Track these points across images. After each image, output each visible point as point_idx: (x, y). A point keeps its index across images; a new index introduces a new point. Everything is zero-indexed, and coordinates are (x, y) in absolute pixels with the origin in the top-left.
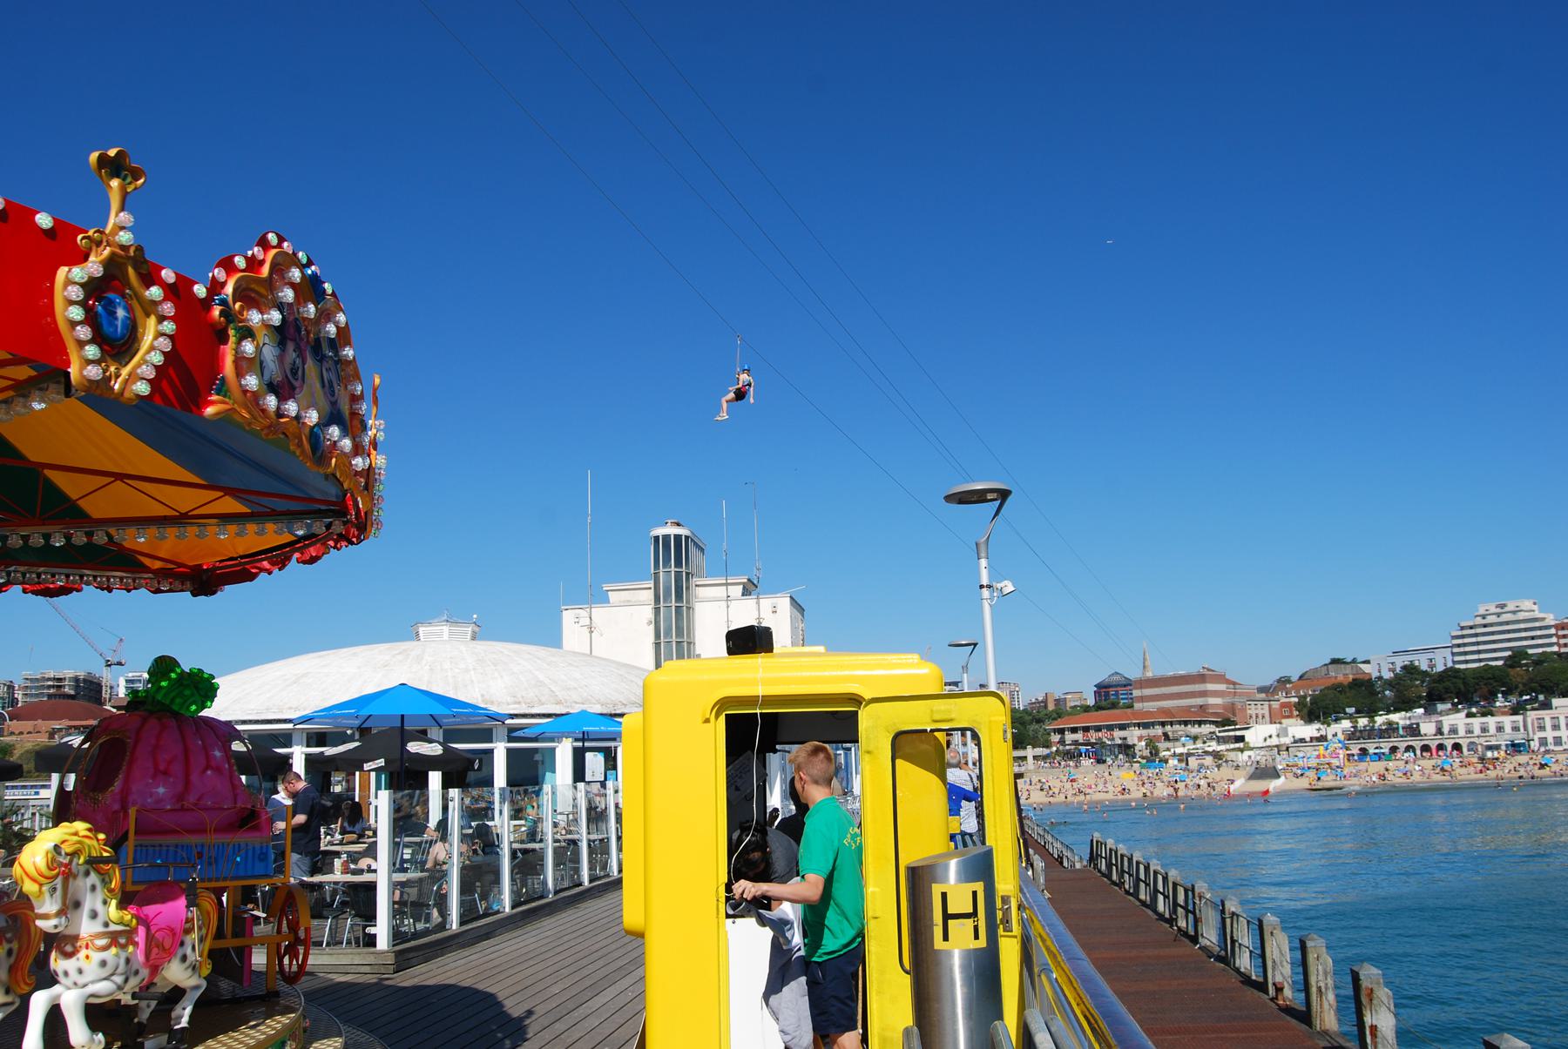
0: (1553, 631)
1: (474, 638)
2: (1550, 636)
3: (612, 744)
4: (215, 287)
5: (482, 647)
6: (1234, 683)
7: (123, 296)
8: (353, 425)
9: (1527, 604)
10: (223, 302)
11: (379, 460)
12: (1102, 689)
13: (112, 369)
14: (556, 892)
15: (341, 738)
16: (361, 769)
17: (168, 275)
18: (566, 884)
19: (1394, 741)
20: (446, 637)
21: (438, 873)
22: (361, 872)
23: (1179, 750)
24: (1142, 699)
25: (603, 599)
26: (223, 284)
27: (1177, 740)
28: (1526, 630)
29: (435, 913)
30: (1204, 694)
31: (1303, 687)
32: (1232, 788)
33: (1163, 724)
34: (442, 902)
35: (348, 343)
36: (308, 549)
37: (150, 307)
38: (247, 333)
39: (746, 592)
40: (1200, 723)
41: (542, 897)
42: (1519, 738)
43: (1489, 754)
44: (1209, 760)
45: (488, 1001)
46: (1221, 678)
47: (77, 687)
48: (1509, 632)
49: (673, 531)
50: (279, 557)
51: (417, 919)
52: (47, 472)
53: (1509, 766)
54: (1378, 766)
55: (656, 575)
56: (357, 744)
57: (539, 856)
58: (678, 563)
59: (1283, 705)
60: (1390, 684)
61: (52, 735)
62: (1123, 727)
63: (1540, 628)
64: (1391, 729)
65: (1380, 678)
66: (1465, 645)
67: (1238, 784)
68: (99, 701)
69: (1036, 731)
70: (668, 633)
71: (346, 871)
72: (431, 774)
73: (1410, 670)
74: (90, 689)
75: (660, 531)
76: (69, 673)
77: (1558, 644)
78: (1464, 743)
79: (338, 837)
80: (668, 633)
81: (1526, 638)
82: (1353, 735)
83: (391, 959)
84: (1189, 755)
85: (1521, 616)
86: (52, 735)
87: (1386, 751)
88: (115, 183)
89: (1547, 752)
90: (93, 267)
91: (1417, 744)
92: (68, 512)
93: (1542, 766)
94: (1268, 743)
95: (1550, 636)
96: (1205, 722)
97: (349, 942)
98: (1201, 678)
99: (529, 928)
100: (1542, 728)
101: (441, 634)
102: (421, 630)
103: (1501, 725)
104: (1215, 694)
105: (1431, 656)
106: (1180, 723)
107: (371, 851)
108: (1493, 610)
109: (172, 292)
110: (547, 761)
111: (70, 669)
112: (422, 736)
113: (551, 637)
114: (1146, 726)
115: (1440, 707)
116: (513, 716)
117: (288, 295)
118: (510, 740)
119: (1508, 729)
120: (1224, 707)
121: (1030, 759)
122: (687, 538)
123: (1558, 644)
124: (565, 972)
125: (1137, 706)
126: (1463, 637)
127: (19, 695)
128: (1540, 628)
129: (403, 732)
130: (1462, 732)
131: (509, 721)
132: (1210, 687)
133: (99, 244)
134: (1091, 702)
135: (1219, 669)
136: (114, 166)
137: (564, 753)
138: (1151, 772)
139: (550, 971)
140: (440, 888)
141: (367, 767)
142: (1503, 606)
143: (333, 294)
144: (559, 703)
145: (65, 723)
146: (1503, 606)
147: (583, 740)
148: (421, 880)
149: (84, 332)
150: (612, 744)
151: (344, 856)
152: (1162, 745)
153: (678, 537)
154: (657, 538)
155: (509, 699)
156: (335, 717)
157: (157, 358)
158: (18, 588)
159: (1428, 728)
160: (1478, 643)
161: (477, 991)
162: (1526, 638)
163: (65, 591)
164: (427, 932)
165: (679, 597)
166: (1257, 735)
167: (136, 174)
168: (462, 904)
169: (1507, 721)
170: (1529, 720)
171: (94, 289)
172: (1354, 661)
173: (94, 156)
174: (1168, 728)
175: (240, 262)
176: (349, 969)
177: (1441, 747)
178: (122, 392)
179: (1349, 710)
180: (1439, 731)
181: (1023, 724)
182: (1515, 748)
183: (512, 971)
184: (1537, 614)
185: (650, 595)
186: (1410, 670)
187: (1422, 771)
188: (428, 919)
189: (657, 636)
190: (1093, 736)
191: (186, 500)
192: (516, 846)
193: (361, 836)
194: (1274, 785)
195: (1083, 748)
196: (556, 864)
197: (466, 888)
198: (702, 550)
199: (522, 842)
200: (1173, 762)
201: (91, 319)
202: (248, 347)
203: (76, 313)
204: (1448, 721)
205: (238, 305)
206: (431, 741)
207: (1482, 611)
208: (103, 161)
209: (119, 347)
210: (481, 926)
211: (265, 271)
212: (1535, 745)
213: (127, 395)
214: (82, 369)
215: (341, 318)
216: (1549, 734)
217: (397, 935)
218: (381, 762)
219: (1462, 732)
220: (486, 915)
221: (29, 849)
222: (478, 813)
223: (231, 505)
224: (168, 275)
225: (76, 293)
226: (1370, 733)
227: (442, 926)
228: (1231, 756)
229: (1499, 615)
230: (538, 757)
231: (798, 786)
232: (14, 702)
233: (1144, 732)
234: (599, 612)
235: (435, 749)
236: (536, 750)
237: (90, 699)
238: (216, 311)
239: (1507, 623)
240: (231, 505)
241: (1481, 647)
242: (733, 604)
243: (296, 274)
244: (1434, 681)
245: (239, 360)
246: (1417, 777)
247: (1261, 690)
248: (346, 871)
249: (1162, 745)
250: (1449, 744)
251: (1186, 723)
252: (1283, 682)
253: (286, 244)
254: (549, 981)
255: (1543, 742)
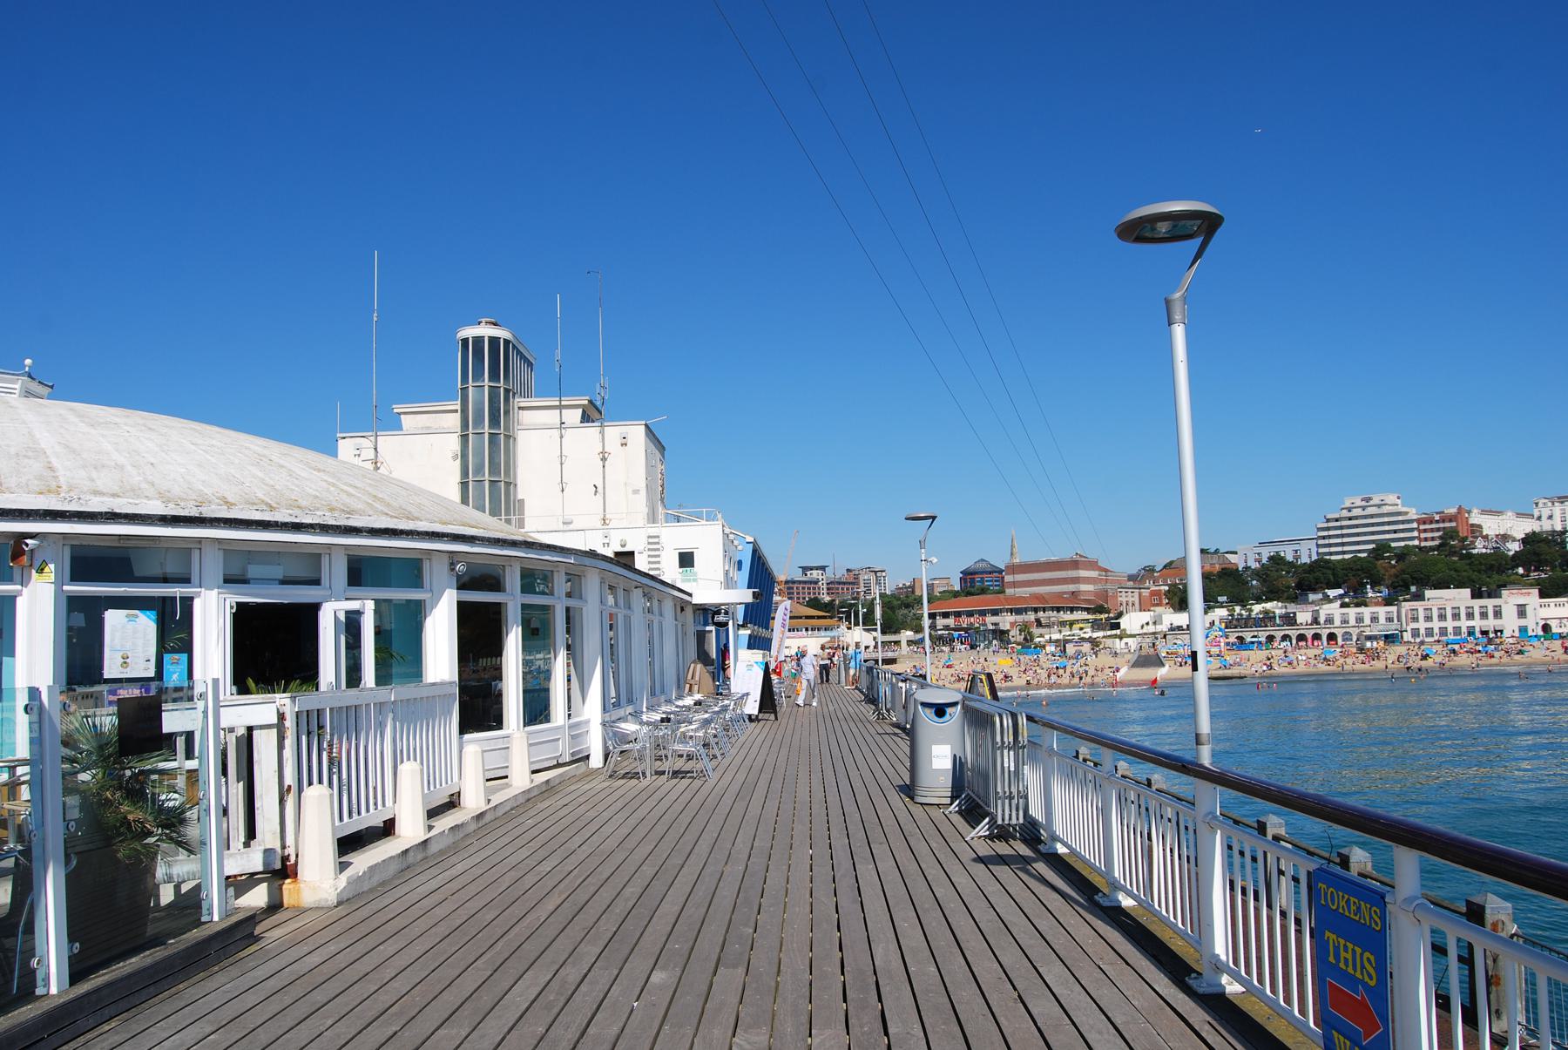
0: (1415, 525)
2: (1412, 530)
3: (177, 591)
6: (1106, 571)
9: (1391, 498)
12: (968, 576)
19: (1270, 630)
23: (1056, 636)
24: (1014, 584)
25: (394, 425)
27: (1048, 626)
28: (1389, 523)
30: (1076, 580)
31: (1169, 576)
32: (1119, 675)
33: (1036, 610)
39: (586, 418)
40: (1072, 610)
42: (1392, 629)
43: (1368, 644)
44: (1086, 647)
46: (1093, 565)
48: (1373, 525)
49: (486, 331)
53: (1391, 658)
54: (1262, 654)
55: (464, 390)
58: (494, 375)
59: (1153, 593)
60: (1257, 574)
62: (995, 613)
63: (1403, 522)
64: (1268, 618)
65: (1247, 568)
66: (1330, 537)
67: (1123, 671)
69: (905, 616)
70: (479, 469)
73: (1276, 560)
75: (470, 332)
77: (1418, 538)
78: (1339, 633)
80: (479, 469)
81: (1388, 532)
82: (1231, 623)
84: (1066, 641)
85: (1386, 509)
87: (1263, 639)
89: (1422, 643)
91: (1294, 633)
93: (1425, 657)
94: (1146, 630)
95: (1412, 530)
96: (1077, 609)
98: (1074, 564)
100: (1415, 619)
103: (1376, 615)
104: (1087, 580)
105: (1296, 547)
106: (1052, 609)
108: (1359, 503)
114: (1018, 611)
115: (1312, 597)
119: (1382, 620)
120: (1096, 594)
121: (904, 644)
122: (507, 342)
123: (1418, 538)
125: (1009, 591)
126: (1328, 529)
128: (1403, 522)
130: (1337, 622)
132: (1083, 573)
134: (957, 587)
135: (1092, 556)
138: (1025, 659)
142: (1368, 500)
146: (1368, 500)
150: (177, 591)
152: (1036, 631)
153: (494, 341)
154: (465, 341)
159: (1303, 617)
160: (1343, 536)
162: (1388, 532)
165: (494, 421)
166: (1133, 621)
169: (1382, 611)
170: (1403, 611)
172: (1217, 551)
174: (1041, 614)
177: (1317, 637)
179: (1220, 599)
180: (1316, 621)
181: (892, 608)
182: (1390, 639)
184: (1401, 509)
185: (454, 420)
186: (1276, 560)
187: (1305, 660)
189: (465, 473)
190: (965, 621)
194: (1161, 673)
195: (956, 634)
198: (530, 364)
200: (1050, 648)
204: (1325, 610)
207: (1348, 505)
212: (1407, 636)
216: (1422, 625)
219: (1337, 622)
226: (1247, 622)
228: (1109, 642)
229: (1364, 508)
231: (658, 455)
233: (1020, 618)
234: (387, 442)
239: (1372, 516)
241: (1346, 540)
242: (568, 434)
244: (1305, 572)
246: (1301, 668)
247: (1131, 578)
249: (1036, 631)
250: (1324, 633)
251: (1058, 609)
252: (1150, 570)
255: (1416, 633)
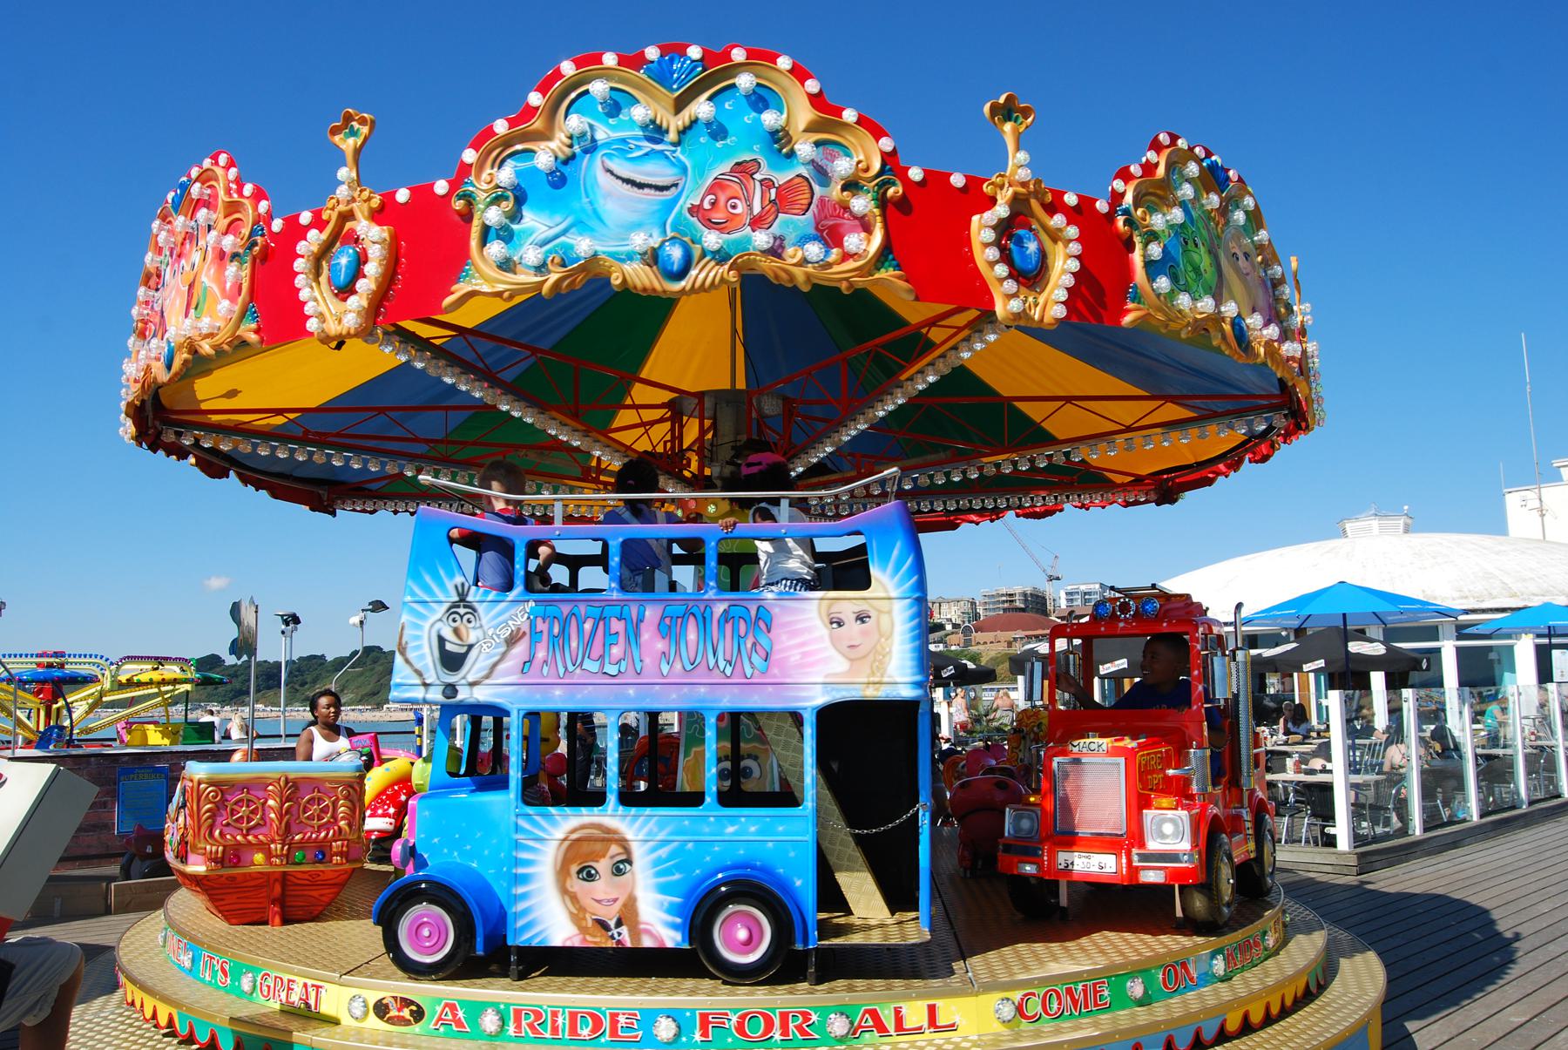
1: (1406, 531)
4: (1117, 197)
5: (1418, 539)
7: (1031, 230)
8: (1277, 313)
10: (1126, 212)
11: (1311, 347)
13: (1031, 299)
14: (1531, 803)
15: (1275, 640)
16: (1300, 670)
17: (1071, 199)
18: (1540, 795)
20: (1376, 530)
21: (1396, 777)
22: (1312, 772)
26: (1123, 195)
29: (1394, 818)
34: (1402, 806)
35: (1260, 226)
36: (1258, 448)
37: (1055, 236)
38: (1152, 236)
41: (1513, 808)
45: (1480, 917)
47: (1026, 601)
50: (1232, 460)
51: (1375, 822)
52: (1017, 404)
56: (1294, 645)
57: (1509, 763)
61: (1010, 644)
68: (1045, 613)
71: (1298, 771)
72: (1373, 674)
74: (1037, 603)
76: (1017, 589)
79: (1281, 737)
83: (1353, 861)
86: (1010, 644)
88: (1008, 127)
90: (1002, 210)
92: (1038, 437)
97: (1307, 842)
99: (1502, 839)
101: (1370, 529)
102: (1348, 526)
107: (1325, 751)
109: (1073, 215)
110: (1504, 660)
111: (1019, 587)
112: (1361, 635)
113: (1495, 524)
116: (1467, 612)
117: (1187, 191)
118: (1459, 638)
124: (1554, 890)
127: (980, 610)
129: (1346, 631)
131: (1461, 618)
133: (1002, 187)
136: (1006, 112)
137: (1524, 651)
139: (1533, 887)
140: (1398, 792)
141: (1306, 667)
143: (1240, 180)
144: (1514, 595)
145: (1019, 634)
147: (1549, 636)
148: (1377, 783)
149: (1002, 270)
151: (1296, 756)
155: (1456, 595)
156: (1276, 617)
157: (1069, 281)
158: (1012, 513)
161: (1469, 906)
163: (1049, 513)
164: (1386, 837)
167: (1026, 113)
168: (1424, 809)
171: (1005, 230)
173: (987, 108)
175: (1135, 169)
176: (1310, 867)
178: (1042, 320)
183: (1486, 885)
188: (1387, 823)
191: (1127, 413)
192: (1479, 751)
193: (1306, 737)
196: (1529, 773)
197: (1427, 794)
199: (1483, 747)
201: (1006, 258)
202: (1155, 250)
203: (993, 253)
205: (1140, 212)
206: (1371, 641)
208: (995, 109)
209: (1031, 277)
210: (1446, 835)
211: (1161, 171)
213: (1046, 320)
214: (1005, 305)
215: (1249, 202)
217: (1358, 839)
218: (1321, 663)
220: (1451, 823)
221: (401, 672)
222: (1433, 714)
223: (1186, 413)
224: (1071, 199)
225: (989, 235)
227: (1404, 831)
230: (1492, 656)
232: (976, 616)
234: (1551, 493)
235: (1378, 649)
236: (1490, 648)
237: (1037, 611)
238: (1120, 221)
240: (1173, 412)
243: (1193, 169)
245: (1149, 264)
248: (1298, 771)
253: (1180, 142)
254: (1535, 898)
